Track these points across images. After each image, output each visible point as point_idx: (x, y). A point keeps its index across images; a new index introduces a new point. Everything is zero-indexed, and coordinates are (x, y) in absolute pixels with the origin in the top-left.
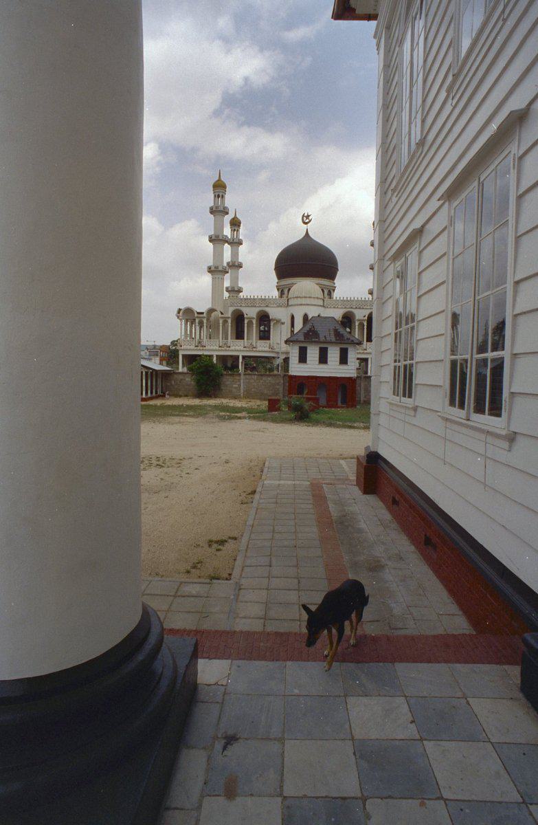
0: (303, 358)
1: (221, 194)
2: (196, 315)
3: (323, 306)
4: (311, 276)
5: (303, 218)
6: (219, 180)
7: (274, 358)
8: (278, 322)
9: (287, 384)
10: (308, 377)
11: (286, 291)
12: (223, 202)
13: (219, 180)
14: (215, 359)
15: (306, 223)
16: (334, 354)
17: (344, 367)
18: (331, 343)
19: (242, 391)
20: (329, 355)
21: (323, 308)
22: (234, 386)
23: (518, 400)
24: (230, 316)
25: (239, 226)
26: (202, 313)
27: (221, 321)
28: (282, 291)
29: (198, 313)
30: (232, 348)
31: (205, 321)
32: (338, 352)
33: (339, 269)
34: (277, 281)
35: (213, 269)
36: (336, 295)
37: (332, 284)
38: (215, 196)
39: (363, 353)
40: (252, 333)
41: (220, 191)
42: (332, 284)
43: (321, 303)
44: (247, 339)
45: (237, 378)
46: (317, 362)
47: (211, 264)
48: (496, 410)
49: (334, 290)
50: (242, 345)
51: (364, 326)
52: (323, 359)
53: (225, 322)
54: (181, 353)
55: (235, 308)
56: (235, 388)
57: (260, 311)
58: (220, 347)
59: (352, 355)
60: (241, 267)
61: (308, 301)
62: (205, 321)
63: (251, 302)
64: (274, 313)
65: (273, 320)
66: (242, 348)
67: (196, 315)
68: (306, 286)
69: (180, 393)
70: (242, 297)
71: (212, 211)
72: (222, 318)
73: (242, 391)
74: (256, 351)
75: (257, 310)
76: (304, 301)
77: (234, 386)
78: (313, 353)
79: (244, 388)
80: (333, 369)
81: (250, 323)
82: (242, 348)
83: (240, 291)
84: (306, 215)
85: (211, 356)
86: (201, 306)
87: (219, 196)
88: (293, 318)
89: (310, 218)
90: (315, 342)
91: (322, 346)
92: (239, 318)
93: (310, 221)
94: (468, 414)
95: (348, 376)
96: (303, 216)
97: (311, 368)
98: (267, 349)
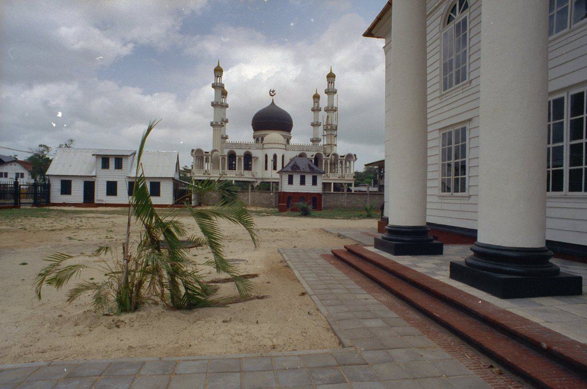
0: (291, 182)
2: (340, 158)
3: (286, 149)
5: (270, 93)
6: (218, 66)
7: (254, 182)
8: (257, 158)
9: (278, 198)
10: (293, 193)
11: (260, 139)
12: (318, 105)
13: (218, 66)
14: (233, 182)
15: (271, 95)
16: (309, 179)
17: (303, 186)
18: (307, 172)
19: (250, 202)
23: (471, 188)
25: (226, 95)
26: (208, 153)
27: (205, 158)
28: (256, 138)
29: (206, 152)
30: (227, 176)
31: (210, 158)
32: (311, 178)
35: (214, 124)
36: (292, 141)
37: (288, 135)
38: (216, 76)
39: (327, 179)
40: (240, 164)
42: (288, 135)
43: (284, 148)
45: (247, 194)
47: (212, 120)
48: (463, 190)
49: (290, 139)
51: (225, 159)
52: (303, 182)
53: (223, 158)
55: (317, 152)
59: (320, 180)
61: (277, 146)
62: (210, 158)
63: (240, 146)
64: (255, 153)
65: (254, 157)
67: (340, 158)
68: (274, 136)
69: (210, 204)
70: (228, 142)
71: (313, 110)
72: (221, 156)
75: (244, 151)
76: (274, 146)
78: (297, 179)
80: (308, 188)
81: (240, 159)
82: (234, 176)
83: (226, 138)
84: (272, 90)
85: (232, 181)
86: (208, 148)
87: (218, 77)
88: (266, 156)
89: (275, 92)
90: (298, 172)
91: (315, 175)
92: (232, 156)
94: (452, 193)
95: (317, 192)
96: (270, 91)
97: (296, 187)
98: (250, 176)
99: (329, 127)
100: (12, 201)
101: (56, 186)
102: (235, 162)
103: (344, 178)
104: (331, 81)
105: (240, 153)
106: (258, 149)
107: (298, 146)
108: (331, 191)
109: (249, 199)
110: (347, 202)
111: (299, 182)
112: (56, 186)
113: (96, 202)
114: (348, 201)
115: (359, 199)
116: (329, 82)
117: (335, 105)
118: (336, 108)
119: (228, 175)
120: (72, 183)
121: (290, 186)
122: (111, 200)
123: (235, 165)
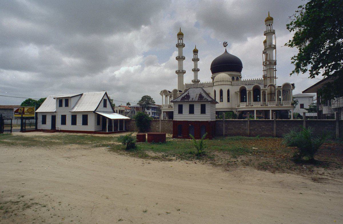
0: (180, 111)
1: (271, 24)
3: (231, 85)
4: (223, 72)
15: (225, 46)
16: (197, 109)
17: (192, 115)
19: (160, 129)
20: (183, 109)
21: (231, 86)
22: (157, 126)
24: (252, 89)
26: (281, 87)
33: (243, 66)
34: (212, 74)
39: (251, 108)
41: (181, 36)
43: (230, 84)
44: (248, 102)
45: (158, 122)
46: (200, 113)
50: (245, 105)
51: (280, 92)
52: (191, 111)
54: (162, 111)
56: (157, 127)
57: (257, 85)
58: (276, 105)
60: (199, 71)
63: (249, 83)
66: (260, 106)
70: (243, 80)
73: (160, 129)
74: (267, 107)
75: (252, 86)
77: (157, 126)
78: (186, 109)
79: (161, 127)
82: (245, 107)
91: (203, 103)
93: (227, 45)
96: (224, 43)
97: (185, 116)
99: (268, 63)
100: (34, 127)
101: (40, 119)
102: (260, 95)
103: (282, 105)
104: (268, 24)
105: (249, 88)
106: (210, 87)
107: (207, 83)
108: (269, 119)
109: (160, 127)
110: (250, 130)
111: (188, 111)
112: (40, 119)
113: (57, 129)
114: (252, 128)
115: (264, 127)
116: (267, 25)
117: (274, 43)
118: (275, 46)
119: (284, 106)
120: (77, 117)
121: (181, 115)
122: (63, 128)
123: (246, 98)
